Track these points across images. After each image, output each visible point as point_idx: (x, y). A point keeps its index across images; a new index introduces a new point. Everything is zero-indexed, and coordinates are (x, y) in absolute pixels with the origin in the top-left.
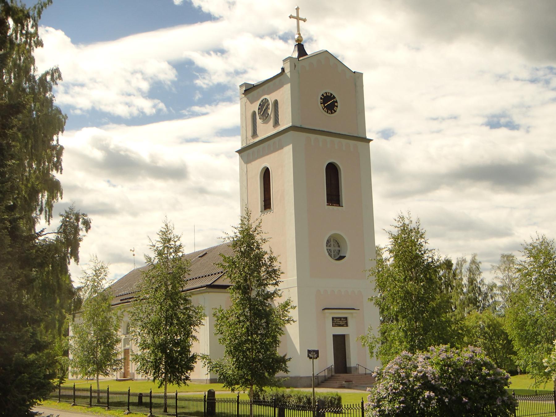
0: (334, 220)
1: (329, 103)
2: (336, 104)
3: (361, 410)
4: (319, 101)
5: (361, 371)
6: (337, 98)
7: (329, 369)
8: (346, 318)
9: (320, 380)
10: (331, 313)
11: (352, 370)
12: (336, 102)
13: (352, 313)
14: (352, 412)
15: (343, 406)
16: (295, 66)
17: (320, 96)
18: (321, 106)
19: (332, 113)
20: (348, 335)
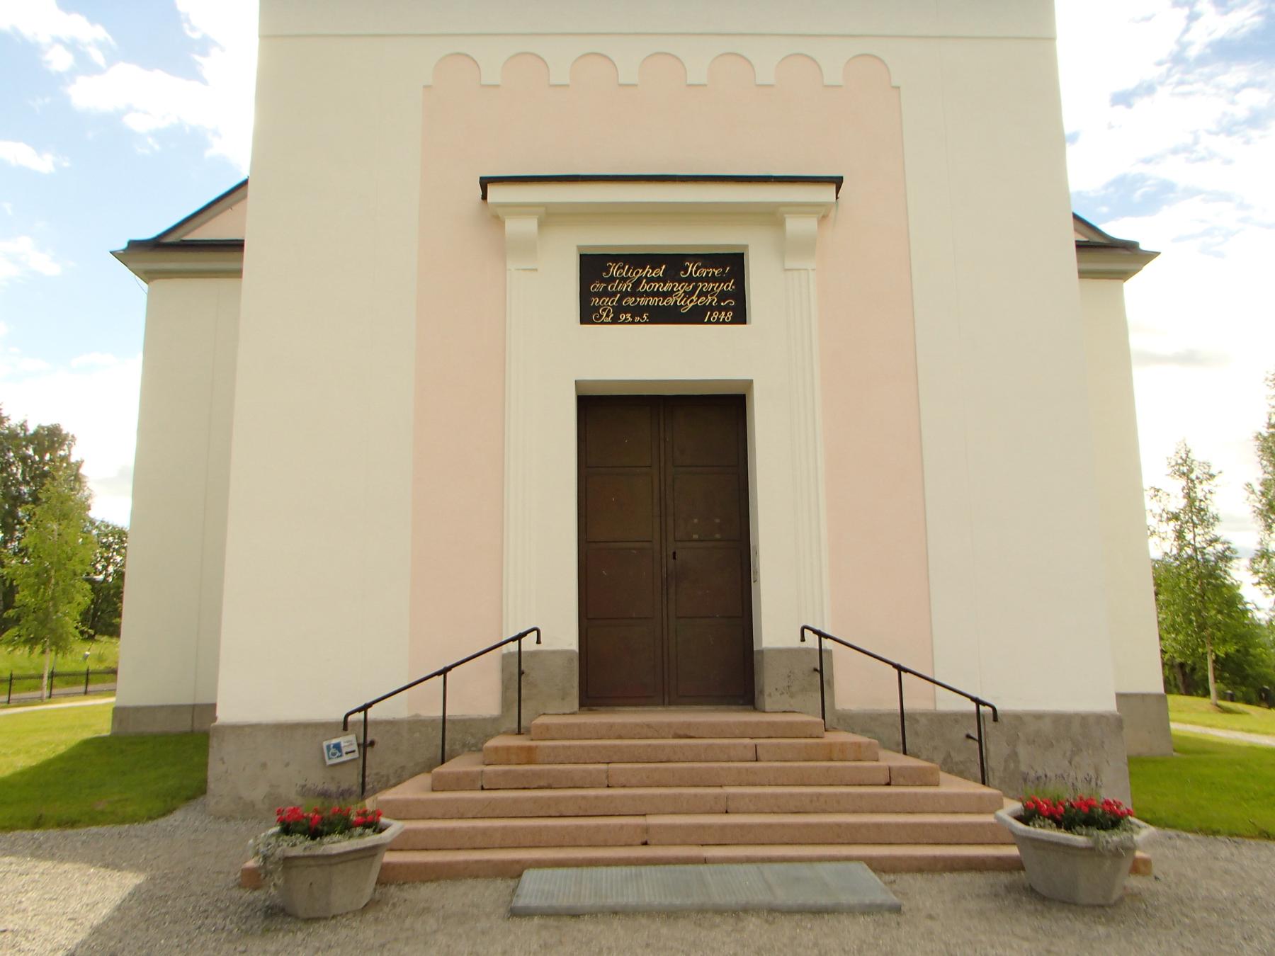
5: (859, 688)
8: (731, 265)
11: (770, 681)
13: (772, 216)
20: (579, 247)
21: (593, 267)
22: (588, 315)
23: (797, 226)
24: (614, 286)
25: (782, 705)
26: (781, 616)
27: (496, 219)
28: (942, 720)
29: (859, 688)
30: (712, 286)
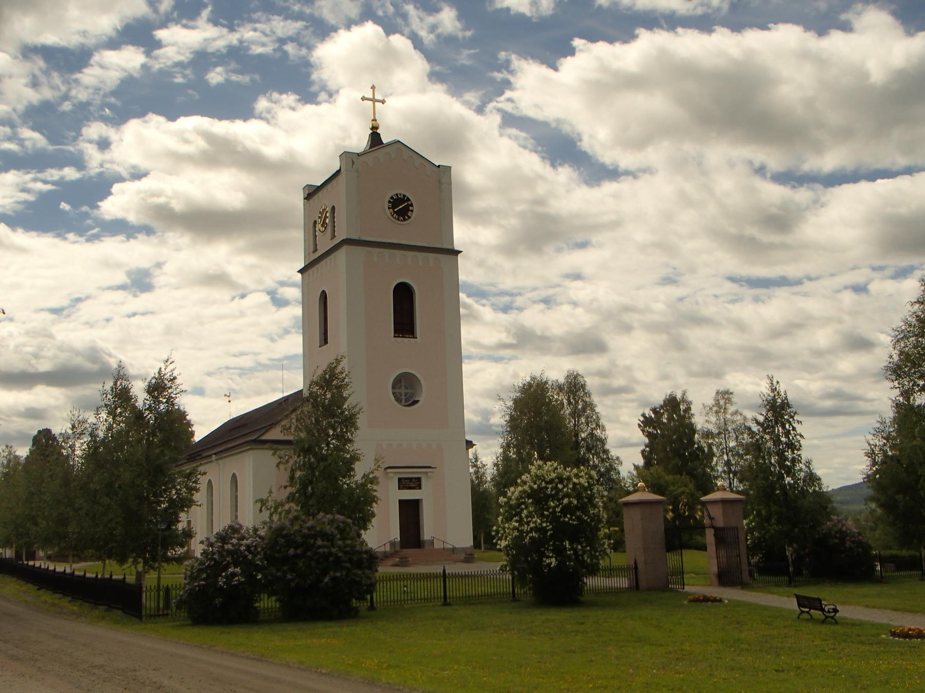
0: (406, 355)
1: (401, 207)
4: (387, 205)
7: (392, 544)
10: (395, 473)
12: (412, 205)
13: (426, 473)
16: (353, 162)
17: (388, 198)
18: (389, 212)
19: (405, 220)
21: (400, 480)
26: (427, 533)
27: (388, 473)
28: (448, 549)
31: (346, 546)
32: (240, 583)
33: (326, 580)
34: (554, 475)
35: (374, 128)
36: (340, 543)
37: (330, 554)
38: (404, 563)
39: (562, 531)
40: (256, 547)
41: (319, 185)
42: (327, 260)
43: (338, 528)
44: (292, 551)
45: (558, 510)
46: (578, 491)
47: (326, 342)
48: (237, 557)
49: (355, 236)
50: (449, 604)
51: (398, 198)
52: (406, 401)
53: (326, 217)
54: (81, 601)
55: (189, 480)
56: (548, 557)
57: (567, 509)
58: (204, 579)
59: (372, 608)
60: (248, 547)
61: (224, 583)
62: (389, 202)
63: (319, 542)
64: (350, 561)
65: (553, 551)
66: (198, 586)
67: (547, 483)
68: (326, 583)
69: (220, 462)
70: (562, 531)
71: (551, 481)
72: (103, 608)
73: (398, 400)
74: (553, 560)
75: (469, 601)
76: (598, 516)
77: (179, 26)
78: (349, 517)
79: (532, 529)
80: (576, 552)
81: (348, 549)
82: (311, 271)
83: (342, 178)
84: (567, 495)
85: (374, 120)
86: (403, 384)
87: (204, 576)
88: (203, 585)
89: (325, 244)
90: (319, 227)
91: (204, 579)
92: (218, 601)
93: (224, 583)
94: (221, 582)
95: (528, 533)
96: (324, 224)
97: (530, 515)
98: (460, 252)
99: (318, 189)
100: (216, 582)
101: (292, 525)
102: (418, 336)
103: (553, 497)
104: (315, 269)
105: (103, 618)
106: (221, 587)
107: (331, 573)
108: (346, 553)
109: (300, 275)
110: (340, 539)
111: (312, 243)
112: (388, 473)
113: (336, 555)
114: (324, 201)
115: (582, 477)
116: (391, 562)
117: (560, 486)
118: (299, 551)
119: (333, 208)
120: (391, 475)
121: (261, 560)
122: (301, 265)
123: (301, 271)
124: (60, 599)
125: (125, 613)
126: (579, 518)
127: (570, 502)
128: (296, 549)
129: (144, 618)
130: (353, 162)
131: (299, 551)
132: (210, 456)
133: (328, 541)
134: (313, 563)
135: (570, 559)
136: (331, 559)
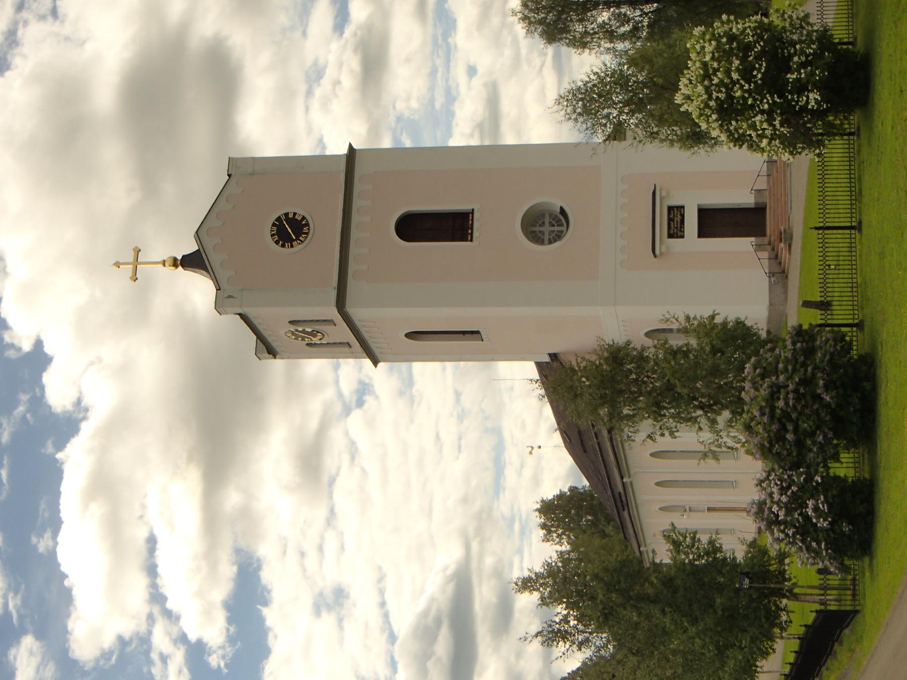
0: (499, 226)
1: (290, 230)
2: (291, 216)
3: (826, 232)
4: (287, 250)
5: (762, 184)
6: (280, 213)
7: (759, 247)
8: (670, 209)
9: (777, 269)
10: (661, 244)
11: (760, 200)
12: (286, 215)
13: (662, 198)
14: (831, 281)
15: (822, 299)
16: (230, 297)
17: (278, 248)
18: (298, 247)
19: (307, 225)
20: (698, 205)
21: (670, 236)
22: (683, 237)
23: (664, 194)
24: (676, 230)
25: (766, 199)
26: (747, 199)
27: (661, 254)
28: (768, 169)
29: (762, 184)
30: (676, 214)
31: (786, 370)
32: (826, 500)
33: (828, 399)
34: (700, 88)
35: (175, 263)
36: (782, 378)
37: (796, 391)
38: (786, 237)
39: (774, 83)
40: (781, 480)
41: (255, 337)
42: (363, 330)
43: (763, 377)
44: (790, 437)
45: (747, 87)
46: (723, 55)
47: (478, 332)
48: (796, 503)
49: (334, 294)
50: (860, 223)
51: (278, 233)
52: (562, 225)
53: (304, 332)
54: (823, 668)
55: (680, 544)
56: (807, 102)
57: (747, 73)
58: (819, 544)
59: (860, 326)
60: (783, 490)
61: (825, 520)
62: (283, 246)
63: (781, 404)
64: (804, 365)
65: (800, 94)
66: (826, 550)
67: (710, 98)
68: (831, 398)
69: (632, 472)
70: (774, 83)
71: (708, 90)
72: (836, 647)
73: (558, 237)
74: (811, 96)
75: (856, 195)
76: (755, 28)
77: (226, 625)
78: (750, 358)
79: (771, 124)
80: (803, 65)
81: (790, 368)
82: (376, 351)
83: (250, 312)
84: (728, 73)
85: (164, 263)
86: (538, 229)
87: (814, 544)
88: (826, 545)
89: (342, 332)
90: (315, 340)
91: (819, 544)
92: (846, 528)
93: (825, 520)
94: (823, 524)
95: (775, 129)
96: (313, 334)
97: (753, 127)
98: (350, 145)
99: (260, 337)
100: (823, 529)
101: (757, 433)
102: (471, 208)
103: (729, 90)
104: (373, 346)
105: (852, 651)
106: (830, 523)
107: (819, 391)
108: (794, 370)
109: (380, 365)
110: (777, 378)
111: (335, 349)
112: (661, 254)
113: (798, 384)
114: (278, 334)
115: (703, 48)
116: (784, 255)
117: (716, 81)
118: (790, 427)
119: (291, 322)
120: (663, 250)
121: (799, 476)
122: (368, 362)
123: (375, 362)
124: (352, 71)
125: (847, 626)
126: (758, 58)
127: (738, 70)
128: (787, 431)
129: (858, 608)
130: (230, 297)
131: (790, 427)
132: (624, 484)
133: (779, 392)
134: (807, 411)
135: (813, 74)
136: (802, 390)
